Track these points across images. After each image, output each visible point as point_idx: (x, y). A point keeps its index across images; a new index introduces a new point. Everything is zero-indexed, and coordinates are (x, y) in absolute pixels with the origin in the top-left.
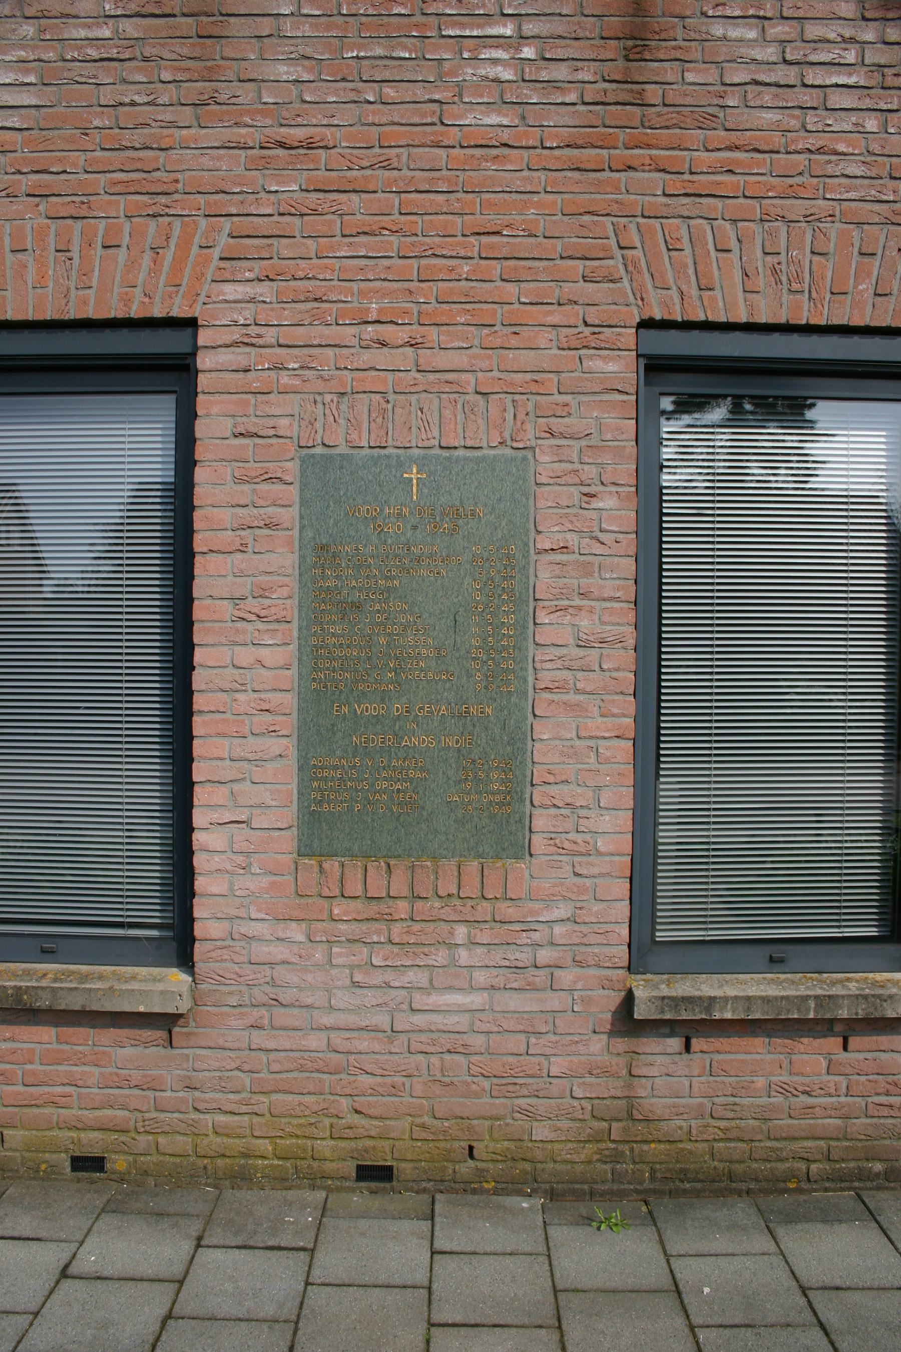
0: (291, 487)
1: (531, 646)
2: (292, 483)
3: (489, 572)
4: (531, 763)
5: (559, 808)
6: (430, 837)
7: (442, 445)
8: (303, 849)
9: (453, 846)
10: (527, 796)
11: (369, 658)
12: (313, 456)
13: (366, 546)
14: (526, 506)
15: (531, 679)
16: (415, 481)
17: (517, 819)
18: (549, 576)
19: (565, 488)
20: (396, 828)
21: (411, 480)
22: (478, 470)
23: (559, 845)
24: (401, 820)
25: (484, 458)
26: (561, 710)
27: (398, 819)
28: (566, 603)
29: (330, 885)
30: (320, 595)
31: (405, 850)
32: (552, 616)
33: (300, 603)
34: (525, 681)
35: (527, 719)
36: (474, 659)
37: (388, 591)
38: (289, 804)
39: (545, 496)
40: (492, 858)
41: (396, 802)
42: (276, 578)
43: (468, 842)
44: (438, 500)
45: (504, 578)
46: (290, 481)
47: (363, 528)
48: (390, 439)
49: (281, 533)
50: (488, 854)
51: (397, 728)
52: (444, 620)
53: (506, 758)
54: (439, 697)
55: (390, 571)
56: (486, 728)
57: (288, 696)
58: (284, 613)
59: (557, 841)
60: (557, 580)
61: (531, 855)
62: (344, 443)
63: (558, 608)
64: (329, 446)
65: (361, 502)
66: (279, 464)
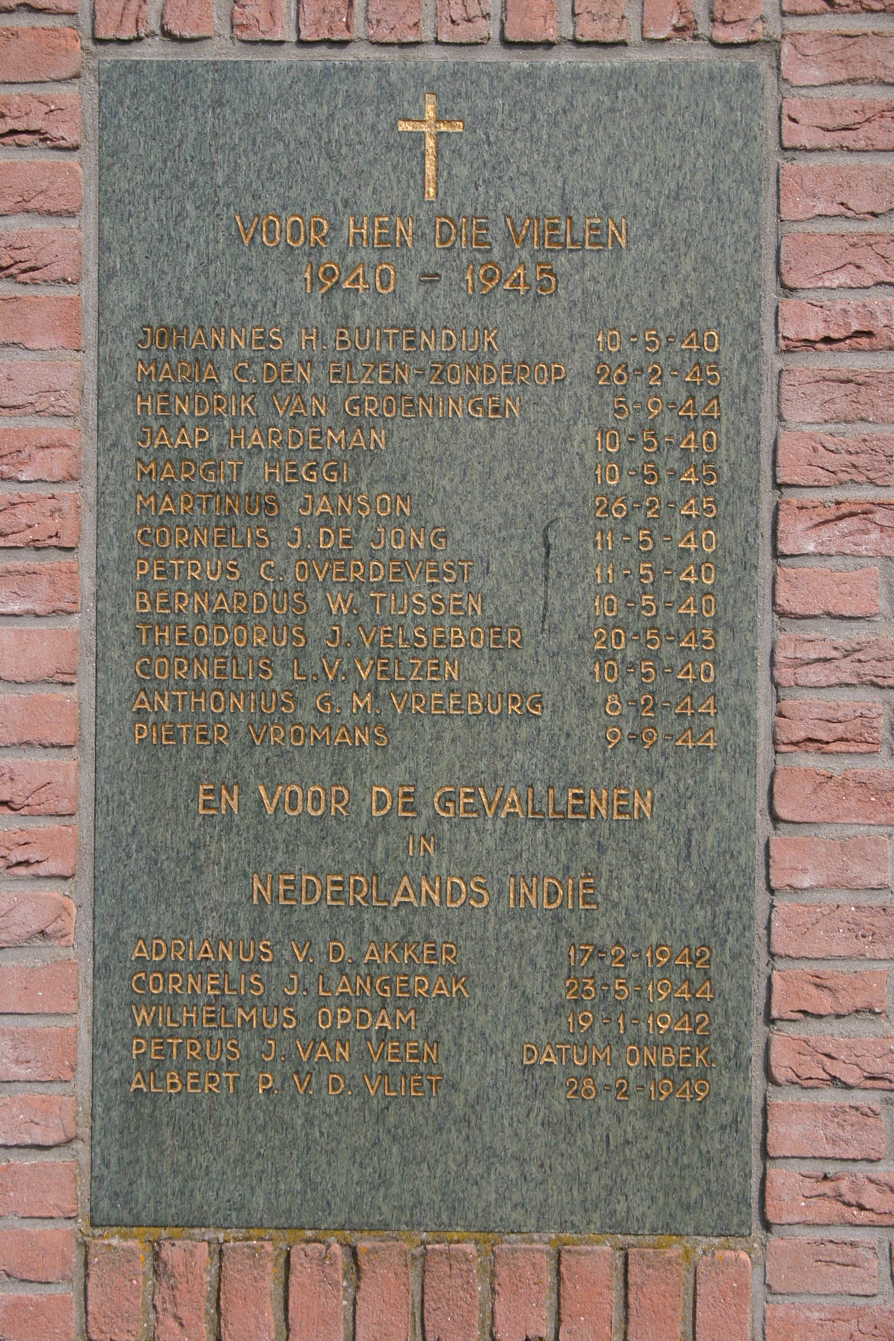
0: (72, 160)
1: (766, 619)
2: (76, 148)
3: (644, 407)
4: (765, 957)
5: (847, 1087)
6: (475, 1169)
7: (510, 36)
8: (105, 1204)
9: (541, 1196)
10: (755, 1052)
11: (300, 655)
12: (135, 68)
13: (289, 331)
14: (751, 216)
15: (763, 714)
16: (430, 143)
17: (725, 1120)
18: (820, 415)
19: (867, 161)
20: (376, 1143)
21: (420, 138)
22: (612, 110)
23: (850, 1197)
24: (392, 1120)
25: (630, 74)
26: (853, 803)
27: (380, 1116)
28: (869, 494)
29: (183, 1312)
30: (159, 473)
31: (401, 1208)
32: (826, 532)
33: (100, 494)
34: (748, 719)
35: (753, 828)
36: (600, 656)
37: (354, 463)
38: (68, 1075)
39: (808, 183)
40: (653, 1232)
41: (376, 1069)
42: (32, 422)
43: (584, 1185)
44: (498, 197)
45: (689, 424)
46: (71, 140)
47: (281, 279)
48: (358, 20)
49: (44, 292)
50: (641, 1220)
51: (379, 853)
52: (515, 545)
53: (694, 942)
54: (500, 765)
55: (359, 403)
56: (636, 856)
57: (66, 760)
58: (54, 524)
59: (844, 1186)
60: (842, 427)
61: (767, 1226)
62: (227, 33)
63: (844, 509)
64: (182, 40)
65: (274, 203)
66: (36, 90)
